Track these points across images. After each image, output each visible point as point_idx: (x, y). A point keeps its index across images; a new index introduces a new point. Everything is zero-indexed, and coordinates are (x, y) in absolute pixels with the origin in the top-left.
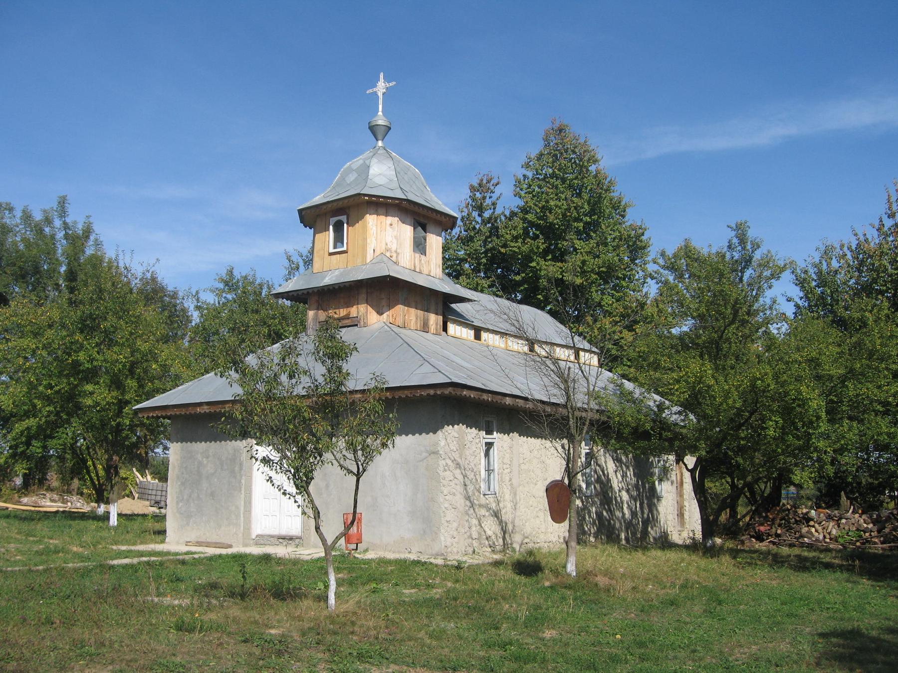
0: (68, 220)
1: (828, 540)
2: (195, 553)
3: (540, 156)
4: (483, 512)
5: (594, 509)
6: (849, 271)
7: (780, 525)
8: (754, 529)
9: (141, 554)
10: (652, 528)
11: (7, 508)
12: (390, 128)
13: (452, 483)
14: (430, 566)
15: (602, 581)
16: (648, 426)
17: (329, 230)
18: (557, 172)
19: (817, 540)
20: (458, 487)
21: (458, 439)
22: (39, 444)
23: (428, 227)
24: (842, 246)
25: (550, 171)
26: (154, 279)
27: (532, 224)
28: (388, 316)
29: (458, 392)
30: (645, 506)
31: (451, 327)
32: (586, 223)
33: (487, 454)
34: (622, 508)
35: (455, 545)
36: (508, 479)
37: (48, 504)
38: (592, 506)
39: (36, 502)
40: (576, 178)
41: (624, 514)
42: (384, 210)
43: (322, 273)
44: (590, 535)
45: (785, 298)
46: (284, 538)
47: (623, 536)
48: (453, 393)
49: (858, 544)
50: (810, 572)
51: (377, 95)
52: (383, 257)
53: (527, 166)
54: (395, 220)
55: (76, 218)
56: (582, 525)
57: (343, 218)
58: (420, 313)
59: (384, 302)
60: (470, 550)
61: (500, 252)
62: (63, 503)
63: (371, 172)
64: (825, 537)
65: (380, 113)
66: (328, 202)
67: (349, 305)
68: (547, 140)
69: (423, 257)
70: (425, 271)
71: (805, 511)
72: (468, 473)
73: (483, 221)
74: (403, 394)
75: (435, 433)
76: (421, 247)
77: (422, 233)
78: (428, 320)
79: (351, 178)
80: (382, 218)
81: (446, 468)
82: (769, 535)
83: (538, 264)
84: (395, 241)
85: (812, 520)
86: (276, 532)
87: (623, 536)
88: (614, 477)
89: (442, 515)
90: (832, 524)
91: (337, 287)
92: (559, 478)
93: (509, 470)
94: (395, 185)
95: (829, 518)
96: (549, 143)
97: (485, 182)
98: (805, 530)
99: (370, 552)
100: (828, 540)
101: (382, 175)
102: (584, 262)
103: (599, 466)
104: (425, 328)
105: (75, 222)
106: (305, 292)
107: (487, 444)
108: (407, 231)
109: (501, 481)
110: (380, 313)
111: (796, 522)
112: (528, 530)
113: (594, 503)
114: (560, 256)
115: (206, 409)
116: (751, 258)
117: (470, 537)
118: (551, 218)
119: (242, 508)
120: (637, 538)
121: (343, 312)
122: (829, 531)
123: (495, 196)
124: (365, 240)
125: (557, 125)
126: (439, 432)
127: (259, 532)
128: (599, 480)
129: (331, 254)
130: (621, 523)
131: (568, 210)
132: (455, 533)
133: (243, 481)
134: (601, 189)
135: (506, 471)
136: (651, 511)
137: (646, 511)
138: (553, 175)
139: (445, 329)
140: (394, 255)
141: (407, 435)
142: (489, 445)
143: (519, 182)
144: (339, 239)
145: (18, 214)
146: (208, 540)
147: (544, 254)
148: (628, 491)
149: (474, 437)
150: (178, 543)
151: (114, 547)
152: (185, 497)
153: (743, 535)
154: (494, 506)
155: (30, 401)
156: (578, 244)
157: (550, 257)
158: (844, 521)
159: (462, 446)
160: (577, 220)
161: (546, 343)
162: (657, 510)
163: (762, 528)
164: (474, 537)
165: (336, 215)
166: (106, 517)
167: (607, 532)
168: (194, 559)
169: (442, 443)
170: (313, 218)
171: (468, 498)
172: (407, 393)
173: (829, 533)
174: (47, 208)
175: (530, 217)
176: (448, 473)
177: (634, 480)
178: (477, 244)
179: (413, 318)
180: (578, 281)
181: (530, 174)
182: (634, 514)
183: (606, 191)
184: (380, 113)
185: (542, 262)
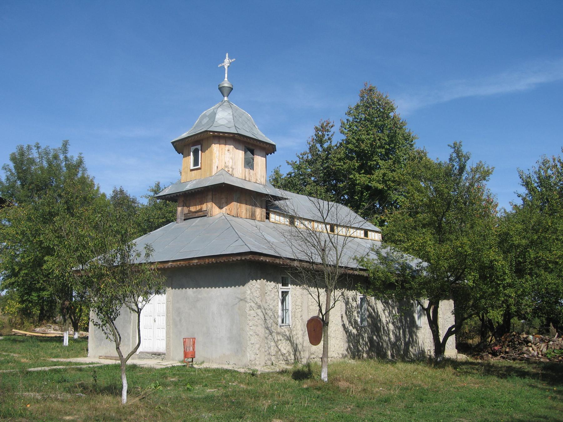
0: (69, 155)
1: (540, 356)
2: (82, 364)
3: (358, 107)
4: (280, 337)
5: (366, 335)
6: (558, 176)
7: (508, 346)
8: (491, 348)
9: (62, 364)
10: (412, 347)
11: (26, 335)
12: (232, 89)
13: (256, 319)
14: (234, 374)
15: (343, 384)
16: (393, 279)
17: (189, 155)
18: (367, 117)
19: (533, 356)
21: (259, 289)
22: (36, 295)
23: (255, 152)
24: (554, 160)
25: (363, 116)
26: (122, 191)
27: (351, 151)
29: (257, 258)
30: (407, 333)
31: (272, 216)
32: (386, 149)
33: (283, 301)
34: (389, 334)
35: (257, 359)
36: (299, 315)
37: (52, 332)
39: (44, 331)
40: (380, 120)
41: (390, 339)
43: (186, 183)
44: (363, 353)
45: (516, 195)
47: (389, 353)
48: (253, 259)
49: (560, 358)
50: (506, 378)
51: (224, 68)
53: (349, 113)
54: (231, 147)
55: (73, 154)
57: (199, 147)
58: (249, 207)
59: (223, 201)
60: (269, 363)
61: (332, 169)
62: (62, 331)
63: (217, 116)
64: (538, 353)
65: (226, 79)
67: (202, 203)
68: (362, 97)
69: (251, 171)
70: (253, 180)
71: (525, 336)
72: (268, 312)
73: (324, 150)
74: (222, 260)
75: (243, 286)
76: (250, 164)
77: (252, 156)
78: (255, 211)
79: (205, 121)
80: (223, 146)
81: (251, 308)
82: (501, 352)
83: (354, 176)
84: (231, 161)
85: (530, 342)
87: (389, 353)
88: (383, 314)
89: (248, 339)
90: (543, 345)
91: (193, 191)
92: (316, 315)
93: (300, 310)
94: (232, 124)
95: (542, 340)
96: (363, 99)
97: (325, 124)
98: (525, 348)
100: (540, 356)
101: (224, 118)
102: (384, 175)
104: (253, 217)
106: (175, 195)
107: (282, 292)
108: (240, 154)
109: (294, 316)
110: (221, 208)
111: (519, 343)
114: (369, 171)
116: (464, 166)
118: (363, 146)
119: (131, 335)
121: (198, 208)
122: (541, 349)
123: (330, 134)
124: (211, 160)
125: (368, 87)
128: (370, 316)
130: (387, 345)
131: (375, 141)
132: (258, 352)
133: (132, 317)
134: (397, 127)
135: (298, 310)
136: (411, 336)
137: (408, 336)
138: (366, 119)
139: (268, 218)
140: (231, 170)
141: (227, 287)
142: (285, 294)
143: (344, 124)
144: (196, 163)
146: (112, 355)
147: (359, 170)
148: (393, 323)
149: (273, 289)
150: (95, 357)
153: (484, 352)
154: (288, 333)
155: (12, 266)
156: (381, 163)
157: (363, 171)
158: (551, 343)
159: (264, 294)
160: (381, 147)
162: (416, 336)
163: (496, 348)
165: (194, 145)
166: (60, 339)
167: (378, 351)
168: (89, 367)
169: (249, 292)
170: (182, 147)
171: (267, 328)
172: (225, 259)
173: (541, 351)
174: (56, 148)
175: (350, 146)
176: (252, 311)
178: (318, 165)
179: (244, 211)
180: (380, 186)
181: (351, 119)
182: (397, 338)
183: (400, 129)
184: (226, 79)
185: (357, 175)
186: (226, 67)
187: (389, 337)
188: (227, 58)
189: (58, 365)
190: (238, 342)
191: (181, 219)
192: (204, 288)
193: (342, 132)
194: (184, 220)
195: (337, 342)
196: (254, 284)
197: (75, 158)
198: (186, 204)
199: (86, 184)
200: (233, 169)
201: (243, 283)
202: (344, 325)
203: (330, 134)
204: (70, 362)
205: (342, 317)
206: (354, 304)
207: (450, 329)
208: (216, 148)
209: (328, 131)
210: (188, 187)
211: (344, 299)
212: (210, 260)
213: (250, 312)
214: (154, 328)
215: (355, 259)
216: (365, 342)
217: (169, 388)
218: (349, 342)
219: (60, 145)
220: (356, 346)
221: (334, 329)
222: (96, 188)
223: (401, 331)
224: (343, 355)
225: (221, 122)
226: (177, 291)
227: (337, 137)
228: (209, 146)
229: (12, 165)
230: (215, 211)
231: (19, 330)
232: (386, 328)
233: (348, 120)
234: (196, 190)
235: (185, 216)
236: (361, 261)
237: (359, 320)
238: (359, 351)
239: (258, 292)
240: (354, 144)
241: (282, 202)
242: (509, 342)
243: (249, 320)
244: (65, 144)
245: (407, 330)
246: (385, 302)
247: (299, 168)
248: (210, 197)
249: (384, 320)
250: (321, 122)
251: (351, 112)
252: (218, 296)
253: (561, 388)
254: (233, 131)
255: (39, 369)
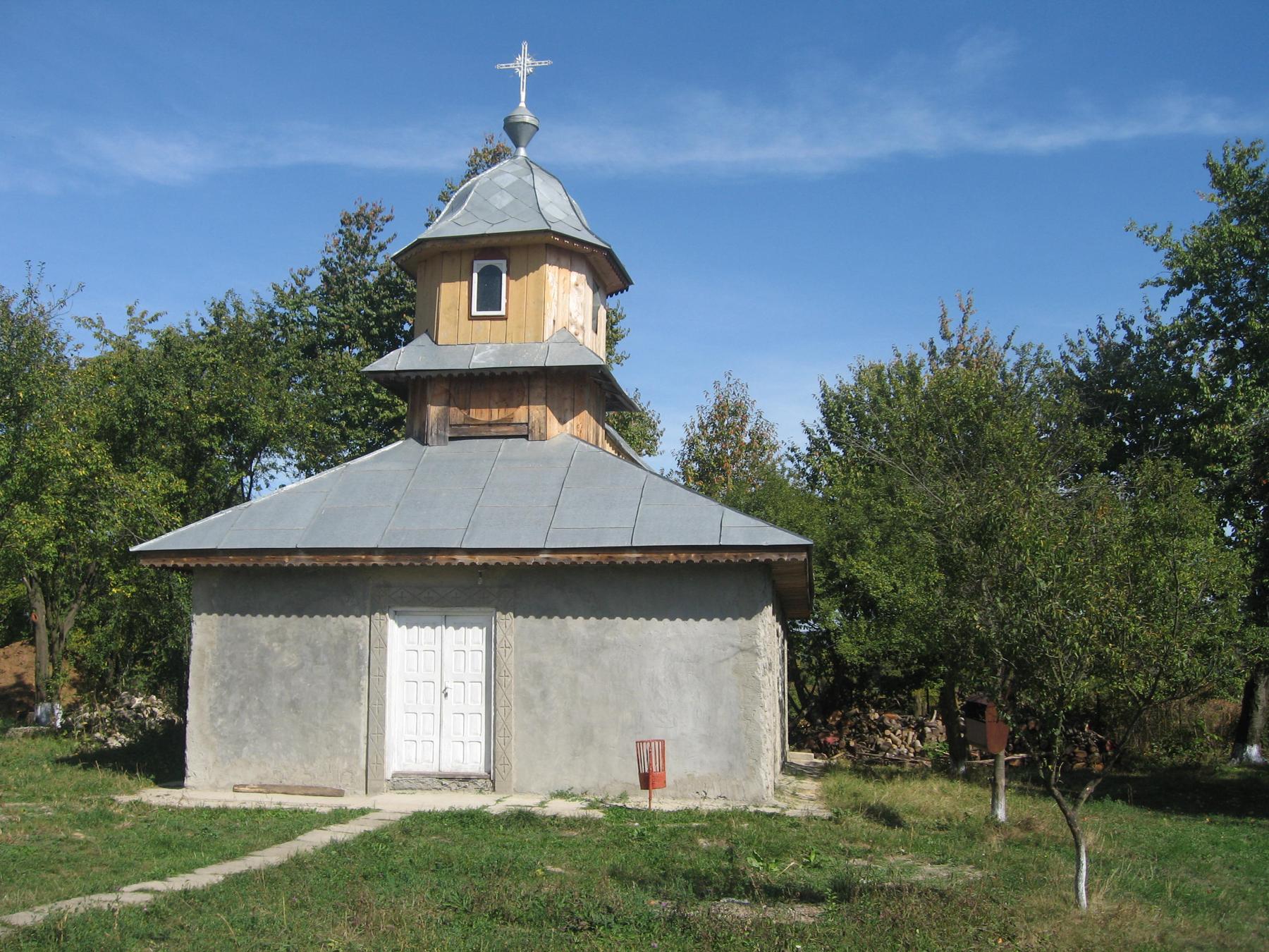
28: (572, 425)
57: (501, 264)
59: (568, 404)
65: (522, 104)
66: (483, 236)
80: (565, 272)
86: (433, 769)
110: (562, 421)
115: (305, 560)
121: (497, 414)
129: (472, 318)
150: (215, 788)
152: (231, 708)
172: (730, 556)
184: (522, 104)
192: (624, 618)
194: (451, 439)
212: (683, 555)
253: (1266, 821)
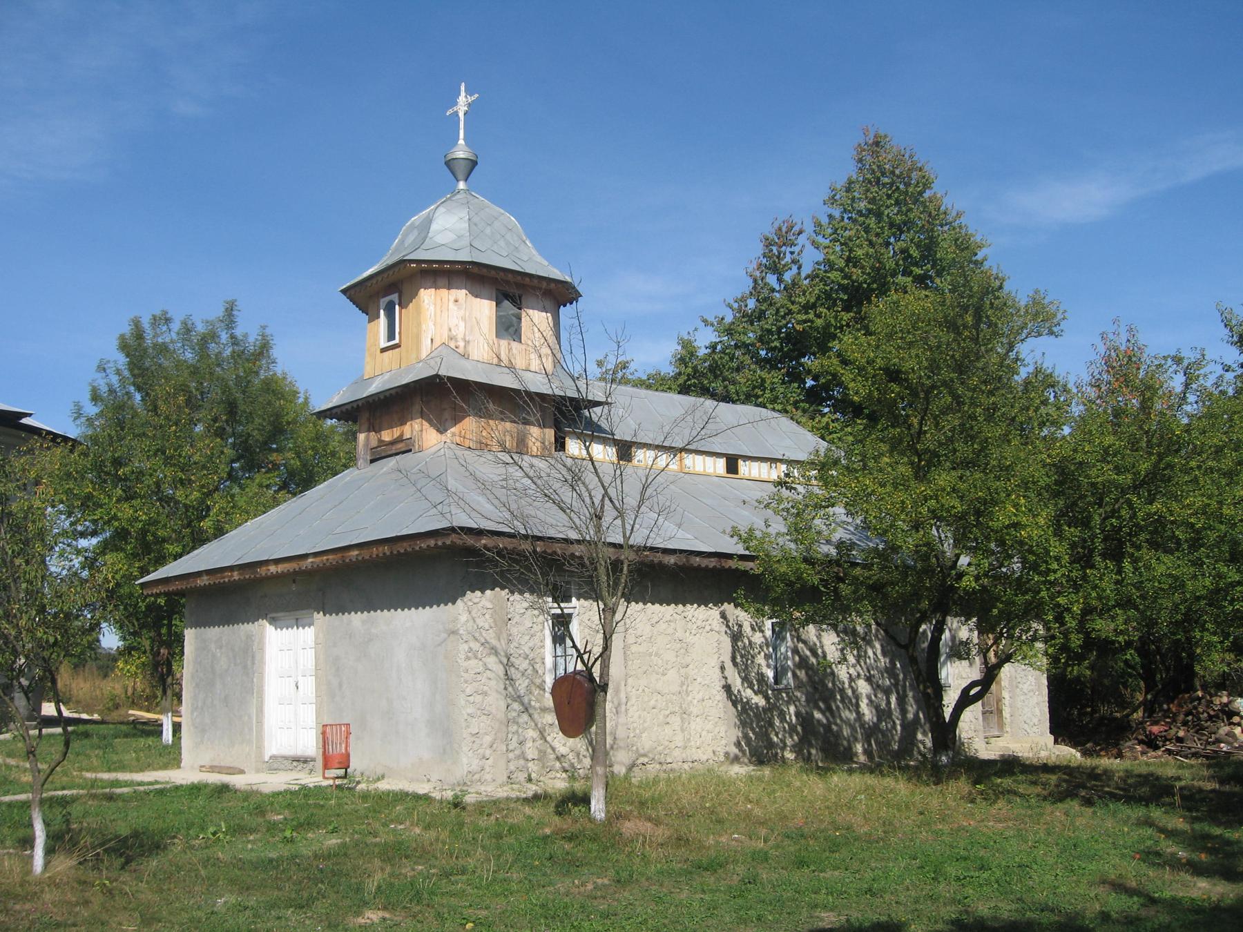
0: (239, 332)
5: (792, 709)
7: (1185, 723)
8: (1144, 729)
12: (474, 163)
17: (378, 317)
20: (493, 683)
21: (478, 609)
28: (454, 435)
34: (858, 706)
38: (788, 703)
41: (860, 715)
42: (445, 281)
44: (783, 749)
46: (296, 760)
47: (859, 748)
52: (449, 347)
54: (461, 294)
55: (248, 329)
56: (767, 735)
60: (522, 777)
65: (461, 142)
67: (403, 423)
69: (515, 345)
71: (1225, 700)
74: (401, 548)
76: (512, 330)
77: (516, 311)
80: (444, 292)
81: (472, 655)
84: (462, 324)
87: (859, 748)
94: (466, 242)
97: (784, 229)
98: (1224, 730)
99: (386, 780)
101: (448, 229)
103: (805, 642)
104: (521, 447)
105: (246, 336)
108: (484, 309)
111: (1210, 718)
112: (646, 743)
113: (791, 700)
117: (523, 756)
120: (890, 752)
121: (396, 432)
124: (419, 325)
126: (459, 601)
127: (274, 752)
130: (853, 728)
139: (560, 445)
140: (461, 344)
143: (820, 225)
145: (176, 326)
146: (223, 764)
148: (869, 679)
151: (88, 775)
159: (503, 621)
161: (781, 461)
164: (530, 757)
165: (386, 290)
167: (825, 746)
176: (473, 662)
177: (883, 661)
181: (837, 213)
184: (461, 142)
186: (461, 115)
187: (858, 713)
188: (463, 94)
189: (70, 788)
190: (444, 729)
191: (365, 460)
193: (816, 246)
194: (372, 461)
195: (710, 726)
196: (476, 600)
197: (253, 339)
198: (374, 427)
199: (276, 390)
200: (467, 342)
201: (451, 597)
202: (727, 688)
203: (796, 249)
204: (117, 780)
205: (723, 668)
206: (758, 638)
207: (966, 691)
208: (427, 297)
209: (793, 244)
210: (373, 388)
211: (728, 626)
213: (466, 664)
214: (277, 704)
215: (735, 533)
216: (790, 724)
217: (251, 838)
218: (743, 724)
219: (220, 312)
220: (764, 735)
221: (700, 696)
222: (301, 400)
223: (893, 699)
224: (727, 754)
225: (440, 239)
226: (333, 619)
227: (809, 257)
228: (415, 294)
229: (122, 360)
230: (426, 436)
231: (148, 711)
232: (849, 692)
233: (830, 216)
234: (387, 394)
235: (372, 454)
236: (747, 539)
237: (770, 674)
238: (771, 745)
239: (487, 616)
240: (842, 270)
241: (598, 410)
242: (1187, 715)
243: (466, 682)
244: (230, 310)
245: (910, 694)
246: (845, 631)
247: (729, 331)
248: (417, 407)
249: (842, 673)
250: (776, 225)
251: (837, 197)
252: (406, 629)
254: (464, 256)
255: (60, 793)
